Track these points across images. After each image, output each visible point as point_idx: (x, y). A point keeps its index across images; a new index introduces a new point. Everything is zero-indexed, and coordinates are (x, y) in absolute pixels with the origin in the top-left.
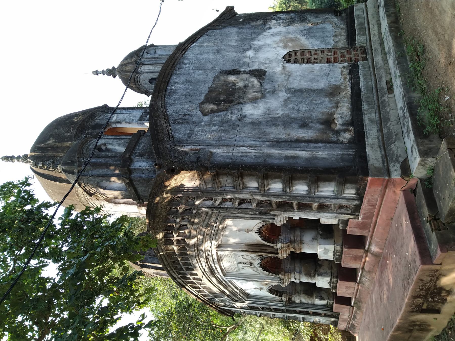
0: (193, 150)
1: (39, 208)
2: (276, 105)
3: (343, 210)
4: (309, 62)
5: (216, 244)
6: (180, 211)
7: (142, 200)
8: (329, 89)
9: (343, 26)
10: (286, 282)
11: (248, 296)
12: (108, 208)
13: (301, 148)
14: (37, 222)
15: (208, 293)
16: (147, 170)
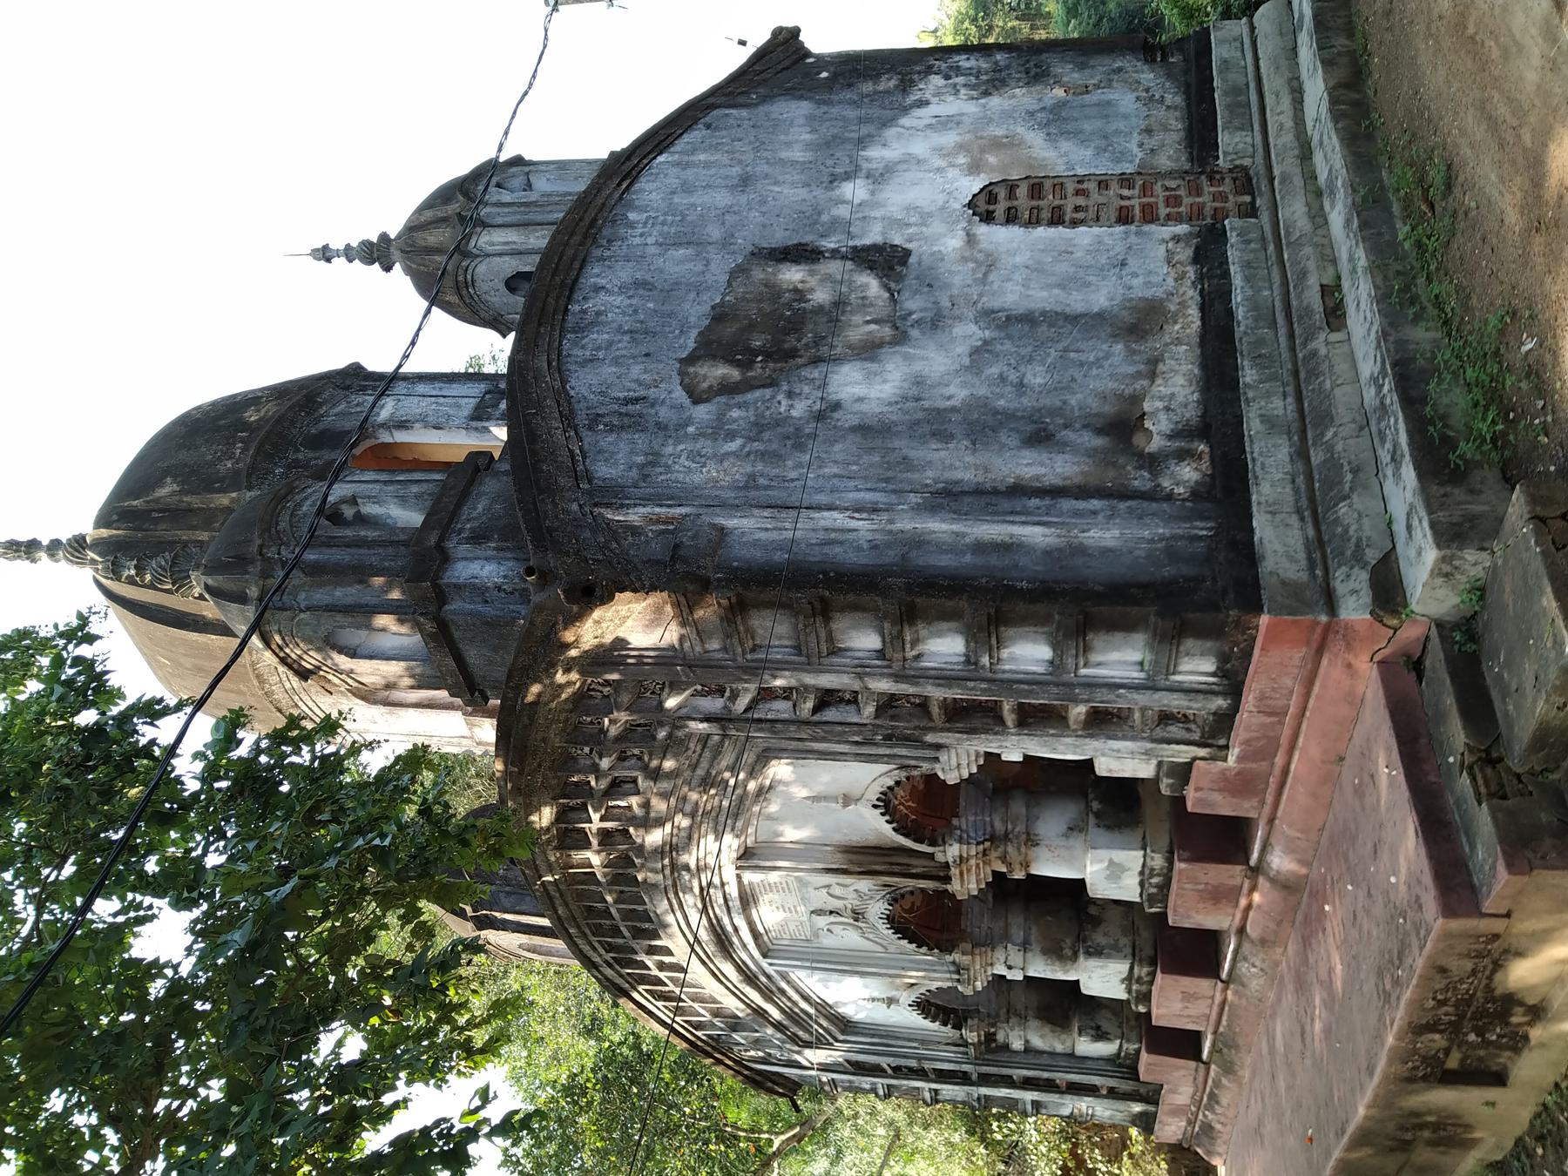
0: (658, 521)
2: (942, 369)
3: (1175, 730)
4: (1056, 219)
5: (735, 846)
6: (614, 731)
8: (1125, 313)
11: (846, 1025)
12: (364, 720)
14: (117, 766)
15: (707, 1017)
16: (499, 589)
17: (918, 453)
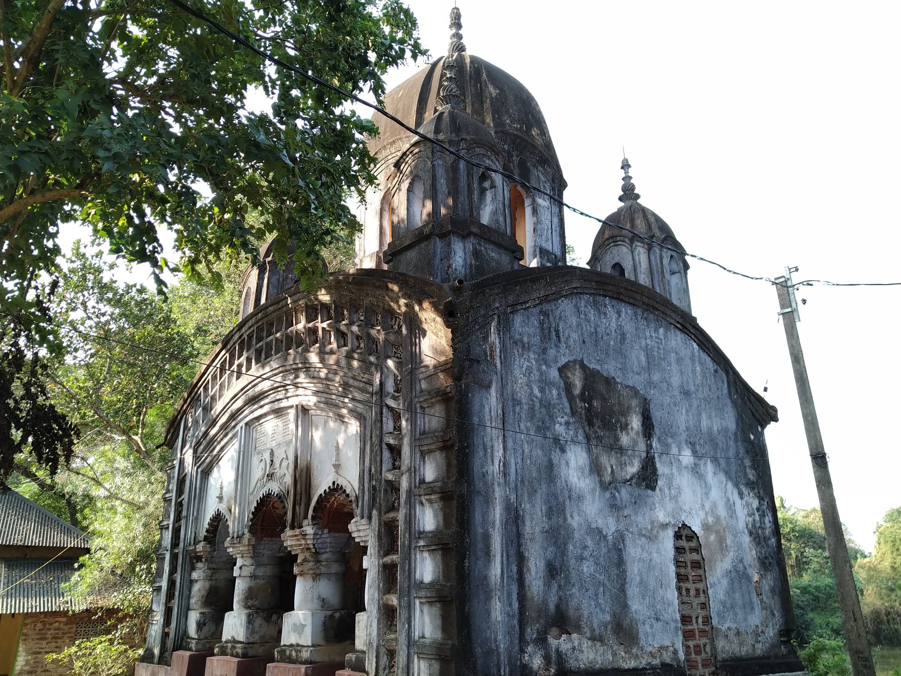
0: (491, 351)
1: (373, 75)
2: (588, 512)
3: (384, 660)
4: (681, 578)
6: (373, 332)
7: (391, 260)
9: (760, 649)
10: (233, 548)
11: (206, 473)
12: (374, 196)
13: (508, 565)
14: (348, 73)
16: (449, 267)
17: (539, 498)
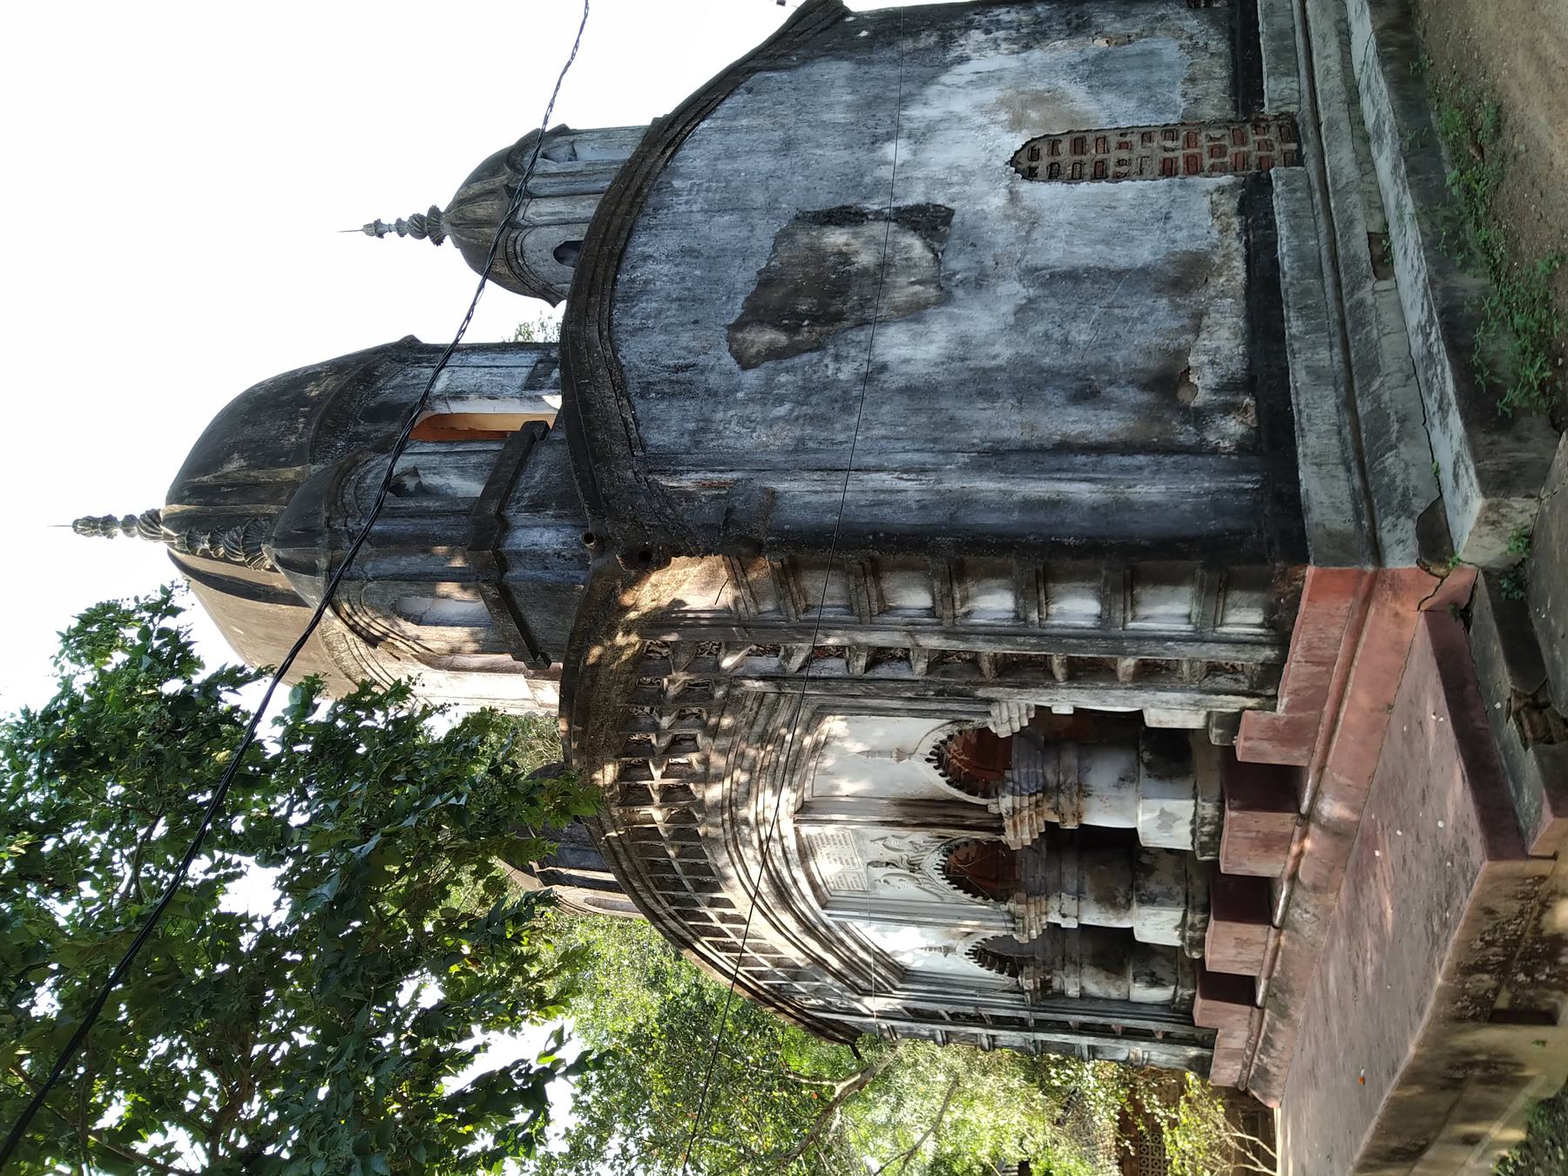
0: (711, 487)
1: (209, 687)
2: (987, 328)
3: (1223, 681)
4: (1099, 174)
6: (673, 691)
7: (544, 656)
9: (1218, 45)
11: (904, 974)
12: (432, 686)
13: (1076, 471)
14: (204, 732)
15: (769, 967)
16: (559, 555)
17: (965, 413)
